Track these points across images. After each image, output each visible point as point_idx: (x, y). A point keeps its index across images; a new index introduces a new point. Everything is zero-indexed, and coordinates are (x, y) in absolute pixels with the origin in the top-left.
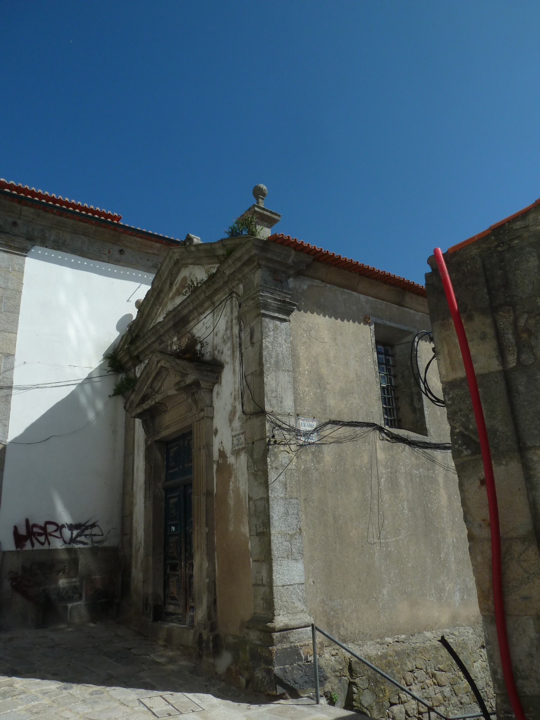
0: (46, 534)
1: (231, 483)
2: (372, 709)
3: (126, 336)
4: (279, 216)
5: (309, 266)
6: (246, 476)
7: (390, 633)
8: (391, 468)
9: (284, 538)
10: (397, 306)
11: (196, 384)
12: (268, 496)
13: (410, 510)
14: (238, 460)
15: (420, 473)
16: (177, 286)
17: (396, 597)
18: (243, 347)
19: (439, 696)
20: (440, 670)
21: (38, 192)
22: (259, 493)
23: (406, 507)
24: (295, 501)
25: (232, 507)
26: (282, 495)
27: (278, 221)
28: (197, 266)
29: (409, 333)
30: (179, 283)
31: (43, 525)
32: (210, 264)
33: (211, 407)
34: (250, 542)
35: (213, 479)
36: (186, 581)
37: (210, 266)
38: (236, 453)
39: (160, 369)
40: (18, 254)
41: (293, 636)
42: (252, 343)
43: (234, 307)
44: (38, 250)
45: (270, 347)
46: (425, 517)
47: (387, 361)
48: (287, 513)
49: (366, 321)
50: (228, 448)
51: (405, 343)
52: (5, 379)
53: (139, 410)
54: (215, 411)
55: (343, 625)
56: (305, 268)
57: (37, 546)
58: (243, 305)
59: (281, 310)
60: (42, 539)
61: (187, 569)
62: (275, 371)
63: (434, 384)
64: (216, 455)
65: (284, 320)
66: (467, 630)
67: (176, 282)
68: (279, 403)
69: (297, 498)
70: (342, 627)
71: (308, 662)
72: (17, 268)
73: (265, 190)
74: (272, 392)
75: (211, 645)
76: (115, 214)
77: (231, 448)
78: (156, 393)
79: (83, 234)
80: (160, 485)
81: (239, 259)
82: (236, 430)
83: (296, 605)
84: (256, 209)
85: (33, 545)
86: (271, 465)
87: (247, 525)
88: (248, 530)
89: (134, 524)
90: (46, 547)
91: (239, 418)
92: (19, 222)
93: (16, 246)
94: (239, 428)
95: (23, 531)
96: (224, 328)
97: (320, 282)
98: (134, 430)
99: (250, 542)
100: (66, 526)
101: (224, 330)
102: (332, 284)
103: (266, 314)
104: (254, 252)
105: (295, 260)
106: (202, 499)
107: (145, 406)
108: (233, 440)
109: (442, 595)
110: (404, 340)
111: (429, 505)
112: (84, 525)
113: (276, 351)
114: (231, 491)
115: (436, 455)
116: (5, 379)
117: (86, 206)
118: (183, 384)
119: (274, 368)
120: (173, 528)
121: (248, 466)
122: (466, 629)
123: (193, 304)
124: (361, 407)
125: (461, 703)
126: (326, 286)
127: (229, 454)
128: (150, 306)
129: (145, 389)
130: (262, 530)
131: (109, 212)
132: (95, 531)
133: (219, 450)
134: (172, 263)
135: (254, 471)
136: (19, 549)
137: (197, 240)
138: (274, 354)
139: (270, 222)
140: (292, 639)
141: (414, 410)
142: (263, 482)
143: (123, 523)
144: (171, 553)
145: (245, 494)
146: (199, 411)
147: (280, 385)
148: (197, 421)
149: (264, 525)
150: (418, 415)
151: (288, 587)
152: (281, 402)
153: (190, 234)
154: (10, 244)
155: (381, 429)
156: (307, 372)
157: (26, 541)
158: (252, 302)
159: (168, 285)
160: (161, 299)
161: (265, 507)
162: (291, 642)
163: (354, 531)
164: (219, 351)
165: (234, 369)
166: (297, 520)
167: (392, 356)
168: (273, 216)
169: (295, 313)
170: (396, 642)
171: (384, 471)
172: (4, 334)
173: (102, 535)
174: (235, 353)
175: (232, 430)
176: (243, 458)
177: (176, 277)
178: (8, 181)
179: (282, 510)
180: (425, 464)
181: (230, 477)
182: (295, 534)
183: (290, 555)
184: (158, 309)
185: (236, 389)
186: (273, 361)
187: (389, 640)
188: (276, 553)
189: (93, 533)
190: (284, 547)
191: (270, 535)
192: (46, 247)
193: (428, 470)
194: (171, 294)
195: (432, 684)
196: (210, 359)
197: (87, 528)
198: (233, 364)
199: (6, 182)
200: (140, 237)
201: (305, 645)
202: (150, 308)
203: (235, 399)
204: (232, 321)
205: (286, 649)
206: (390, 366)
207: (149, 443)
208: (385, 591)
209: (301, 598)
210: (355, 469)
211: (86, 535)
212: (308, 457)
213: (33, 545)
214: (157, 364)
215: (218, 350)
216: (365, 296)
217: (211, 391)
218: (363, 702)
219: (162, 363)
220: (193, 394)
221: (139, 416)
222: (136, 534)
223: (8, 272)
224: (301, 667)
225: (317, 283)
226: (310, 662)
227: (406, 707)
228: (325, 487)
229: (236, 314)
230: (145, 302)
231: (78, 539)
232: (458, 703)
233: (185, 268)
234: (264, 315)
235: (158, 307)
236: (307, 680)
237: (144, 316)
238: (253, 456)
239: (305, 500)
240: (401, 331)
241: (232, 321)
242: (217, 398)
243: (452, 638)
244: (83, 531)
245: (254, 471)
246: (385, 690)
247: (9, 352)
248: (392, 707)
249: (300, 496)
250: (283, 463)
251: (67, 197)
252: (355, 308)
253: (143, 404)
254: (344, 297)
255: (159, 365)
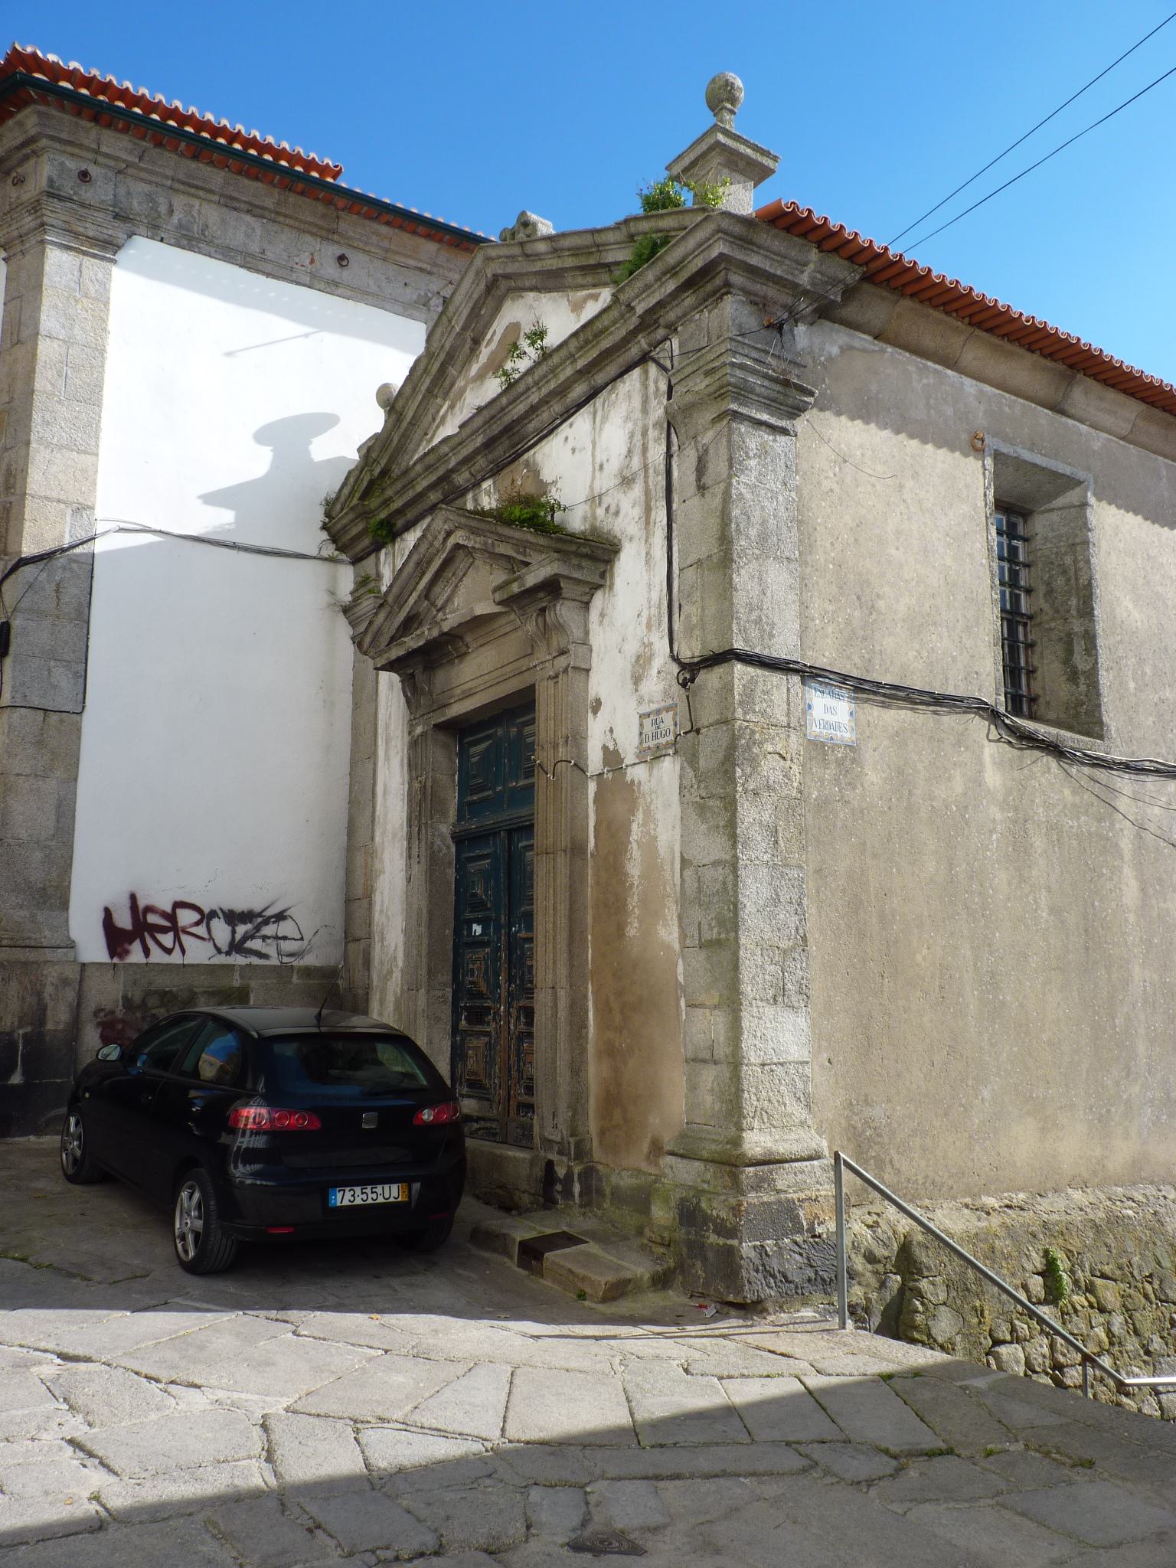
0: (175, 928)
1: (634, 827)
2: (953, 1349)
3: (357, 472)
4: (775, 159)
5: (849, 293)
6: (676, 809)
7: (993, 1187)
8: (1016, 809)
9: (768, 956)
10: (1050, 413)
11: (551, 588)
12: (735, 857)
13: (1054, 910)
14: (655, 772)
15: (1079, 826)
16: (493, 346)
17: (1010, 1108)
18: (676, 497)
19: (1101, 1332)
20: (1104, 1276)
21: (140, 94)
22: (710, 847)
23: (1043, 903)
24: (794, 873)
25: (636, 883)
26: (766, 857)
27: (773, 171)
28: (548, 295)
29: (1072, 483)
30: (497, 338)
31: (168, 909)
32: (583, 287)
33: (584, 644)
34: (680, 962)
35: (587, 817)
36: (510, 1047)
37: (585, 293)
38: (652, 756)
39: (451, 551)
40: (94, 256)
41: (784, 1178)
42: (702, 488)
43: (652, 397)
44: (142, 248)
45: (748, 496)
46: (1086, 931)
47: (1013, 551)
48: (776, 901)
49: (976, 447)
50: (628, 745)
51: (1060, 509)
52: (75, 566)
53: (396, 652)
54: (594, 654)
55: (891, 1161)
56: (839, 299)
57: (157, 956)
58: (678, 390)
59: (778, 406)
60: (167, 939)
61: (512, 1021)
62: (757, 559)
63: (1125, 614)
64: (595, 761)
65: (784, 432)
66: (1164, 1193)
67: (488, 337)
68: (766, 637)
69: (800, 867)
70: (888, 1166)
71: (814, 1236)
72: (92, 293)
73: (738, 87)
74: (751, 610)
75: (577, 1188)
76: (327, 161)
77: (636, 741)
78: (438, 611)
79: (248, 212)
80: (445, 829)
81: (672, 271)
82: (651, 702)
83: (789, 1110)
84: (721, 137)
85: (147, 952)
86: (743, 785)
87: (676, 923)
88: (676, 935)
89: (377, 916)
90: (176, 958)
91: (659, 672)
92: (94, 170)
93: (91, 234)
94: (658, 696)
95: (124, 920)
96: (624, 451)
97: (869, 338)
98: (376, 700)
99: (680, 962)
100: (221, 915)
101: (623, 457)
102: (900, 347)
103: (742, 414)
104: (719, 248)
105: (818, 276)
106: (559, 860)
107: (412, 642)
108: (641, 725)
109: (1113, 1109)
110: (1060, 502)
111: (1096, 903)
112: (260, 915)
113: (763, 508)
114: (634, 845)
115: (1119, 785)
116: (75, 566)
117: (255, 137)
118: (515, 588)
119: (757, 551)
120: (477, 929)
121: (682, 787)
122: (1160, 1191)
123: (540, 389)
124: (954, 659)
125: (1148, 1353)
126: (883, 351)
127: (629, 758)
128: (420, 397)
129: (411, 601)
130: (715, 936)
131: (312, 155)
132: (285, 928)
133: (605, 748)
134: (482, 286)
135: (698, 799)
136: (116, 960)
137: (546, 227)
138: (756, 518)
139: (756, 172)
140: (780, 1185)
141: (1073, 676)
142: (722, 824)
143: (348, 918)
144: (471, 983)
145: (672, 851)
146: (555, 654)
147: (769, 594)
148: (550, 678)
149: (721, 922)
150: (1083, 688)
151: (774, 1067)
152: (771, 636)
153: (529, 213)
154: (74, 228)
155: (994, 716)
156: (831, 566)
157: (131, 942)
158: (707, 382)
159: (468, 344)
160: (447, 382)
161: (724, 883)
162: (778, 1191)
163: (925, 951)
164: (607, 509)
165: (647, 554)
166: (797, 917)
167: (1026, 540)
168: (759, 159)
169: (811, 414)
170: (1008, 1206)
171: (998, 816)
172: (68, 454)
173: (302, 939)
174: (653, 513)
175: (640, 702)
176: (669, 768)
177: (488, 324)
178: (66, 63)
179: (766, 892)
180: (1092, 804)
181: (632, 811)
182: (793, 949)
183: (779, 996)
184: (441, 407)
185: (652, 603)
186: (753, 532)
187: (990, 1201)
188: (749, 989)
189: (280, 935)
190: (767, 977)
191: (738, 946)
192: (162, 240)
193: (1100, 820)
194: (474, 369)
195: (1086, 1304)
196: (583, 528)
197: (266, 922)
198: (646, 541)
199: (61, 63)
200: (387, 223)
201: (810, 1198)
202: (420, 403)
203: (649, 626)
204: (645, 433)
205: (769, 1204)
206: (1017, 564)
207: (419, 730)
208: (986, 1093)
209: (800, 1094)
210: (933, 807)
211: (264, 938)
212: (828, 772)
213: (147, 952)
214: (445, 539)
215: (604, 506)
216: (974, 382)
217: (586, 605)
218: (934, 1332)
219: (459, 537)
220: (543, 610)
221: (390, 667)
222: (382, 939)
223: (72, 301)
224: (800, 1247)
225: (863, 340)
226: (819, 1236)
227: (1028, 1349)
228: (864, 843)
229: (657, 412)
230: (408, 390)
231: (249, 944)
232: (1142, 1352)
233: (513, 300)
234: (736, 416)
235: (439, 400)
236: (813, 1276)
237: (405, 424)
238: (698, 763)
239: (818, 871)
240: (1055, 475)
241: (645, 433)
242: (601, 623)
243: (1131, 1208)
244: (258, 928)
245: (698, 799)
246: (982, 1311)
247: (81, 500)
248: (997, 1349)
249: (806, 862)
250: (771, 782)
251: (210, 111)
252: (950, 411)
253: (406, 636)
254: (925, 381)
255: (451, 541)
